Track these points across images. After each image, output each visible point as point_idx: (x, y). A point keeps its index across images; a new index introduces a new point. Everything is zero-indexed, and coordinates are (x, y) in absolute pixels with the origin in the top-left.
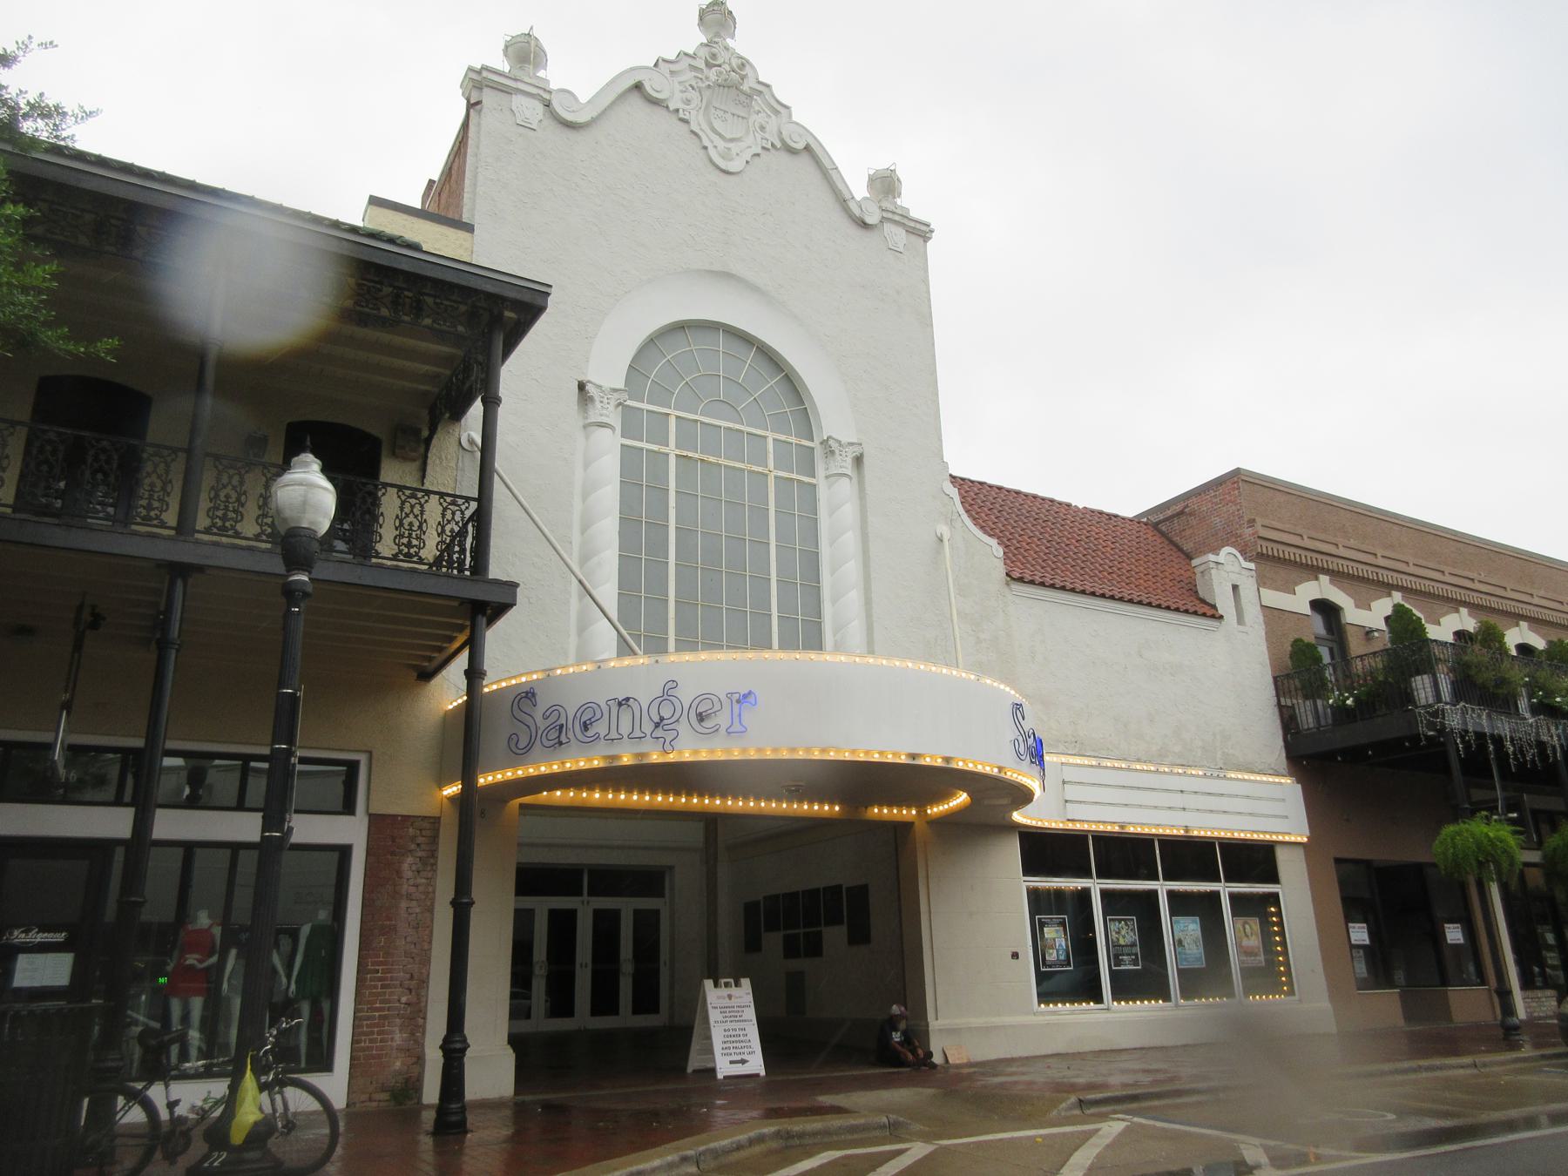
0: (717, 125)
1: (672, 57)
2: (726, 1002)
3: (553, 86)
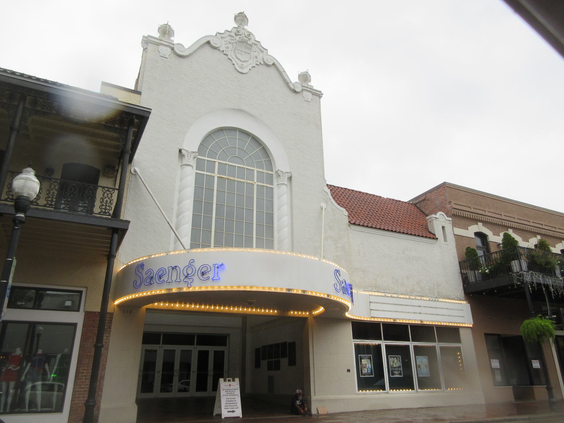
0: (239, 56)
1: (223, 32)
2: (229, 388)
3: (175, 42)
